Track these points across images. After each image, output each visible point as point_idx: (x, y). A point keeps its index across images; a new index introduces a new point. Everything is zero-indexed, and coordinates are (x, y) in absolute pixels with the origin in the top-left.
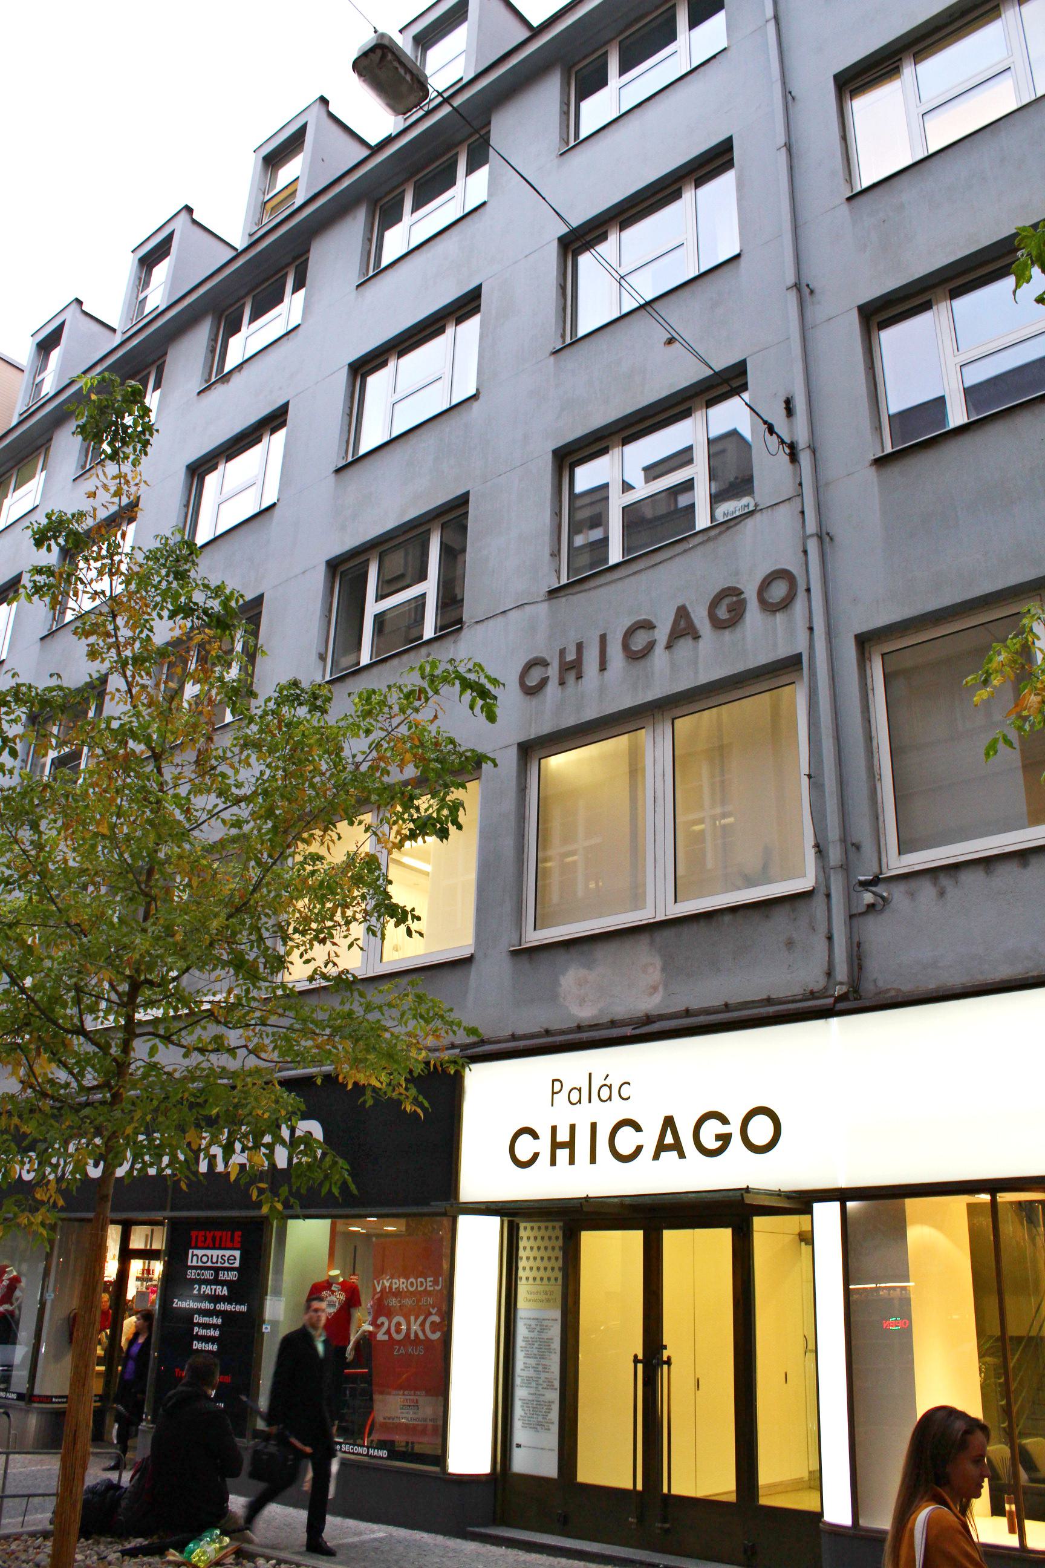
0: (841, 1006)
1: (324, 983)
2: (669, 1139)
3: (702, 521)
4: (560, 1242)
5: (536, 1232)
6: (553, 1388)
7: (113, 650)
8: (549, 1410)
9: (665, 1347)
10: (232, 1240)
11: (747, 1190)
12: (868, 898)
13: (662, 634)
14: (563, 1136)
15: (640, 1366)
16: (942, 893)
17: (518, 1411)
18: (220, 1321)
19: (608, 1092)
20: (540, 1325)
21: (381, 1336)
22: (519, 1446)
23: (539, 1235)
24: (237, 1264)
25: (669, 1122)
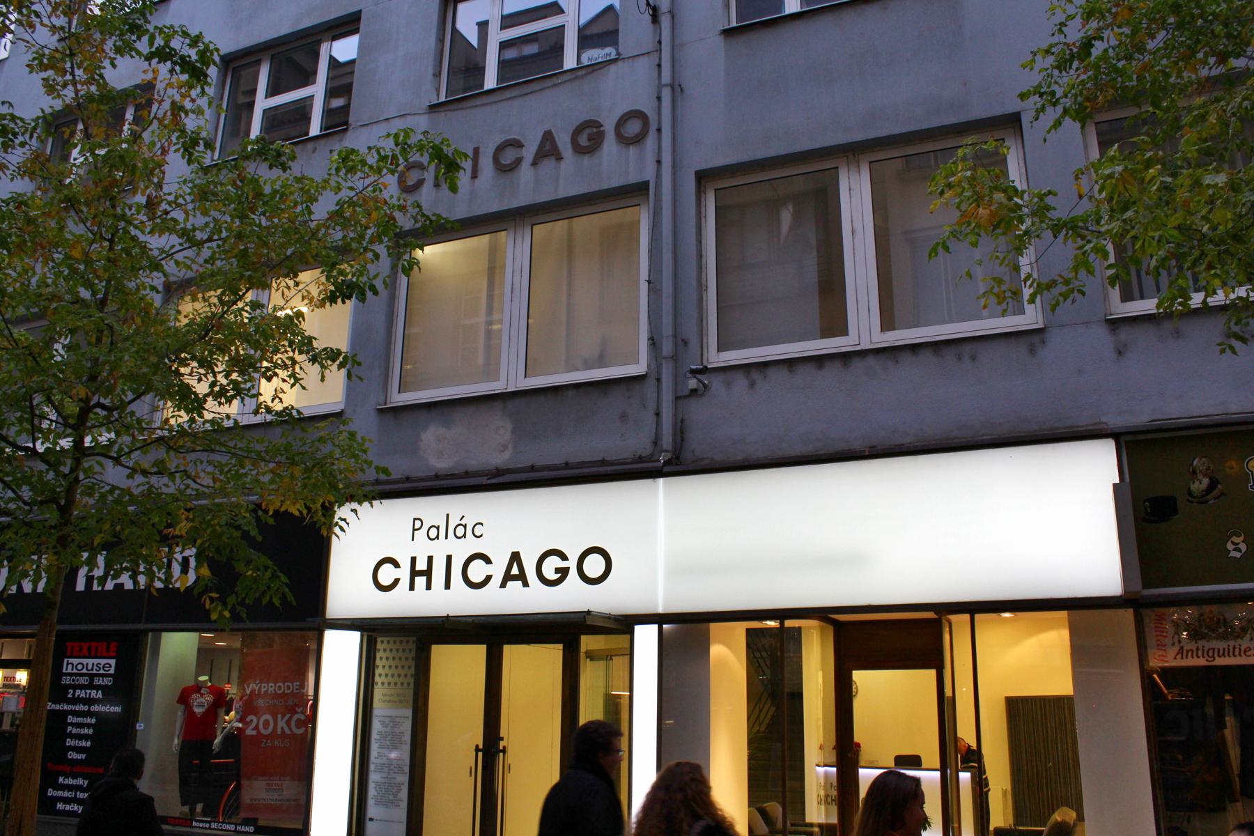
0: (666, 469)
1: (269, 417)
2: (515, 571)
3: (569, 62)
4: (413, 654)
5: (391, 645)
6: (403, 773)
7: (70, 87)
8: (399, 790)
9: (502, 739)
10: (108, 650)
11: (589, 612)
12: (693, 383)
13: (529, 153)
14: (421, 565)
15: (480, 754)
16: (752, 385)
17: (372, 791)
18: (94, 721)
19: (462, 531)
20: (394, 722)
21: (250, 732)
22: (371, 819)
23: (394, 647)
24: (112, 671)
25: (516, 557)
